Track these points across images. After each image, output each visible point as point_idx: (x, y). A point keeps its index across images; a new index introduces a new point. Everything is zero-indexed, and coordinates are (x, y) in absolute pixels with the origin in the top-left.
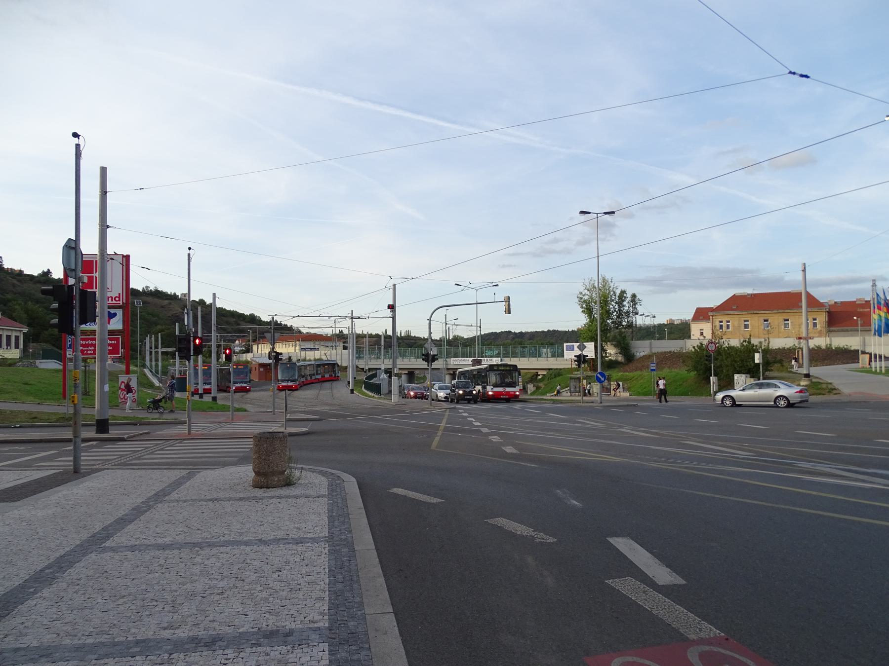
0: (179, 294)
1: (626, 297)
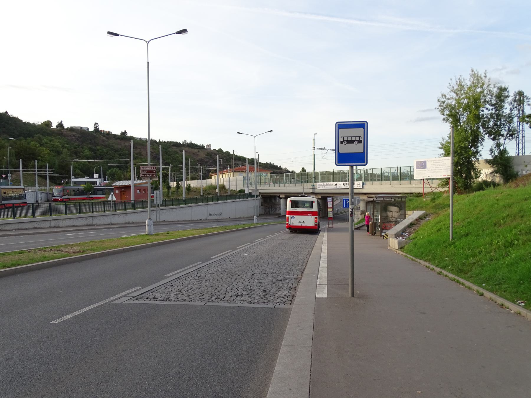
0: (205, 145)
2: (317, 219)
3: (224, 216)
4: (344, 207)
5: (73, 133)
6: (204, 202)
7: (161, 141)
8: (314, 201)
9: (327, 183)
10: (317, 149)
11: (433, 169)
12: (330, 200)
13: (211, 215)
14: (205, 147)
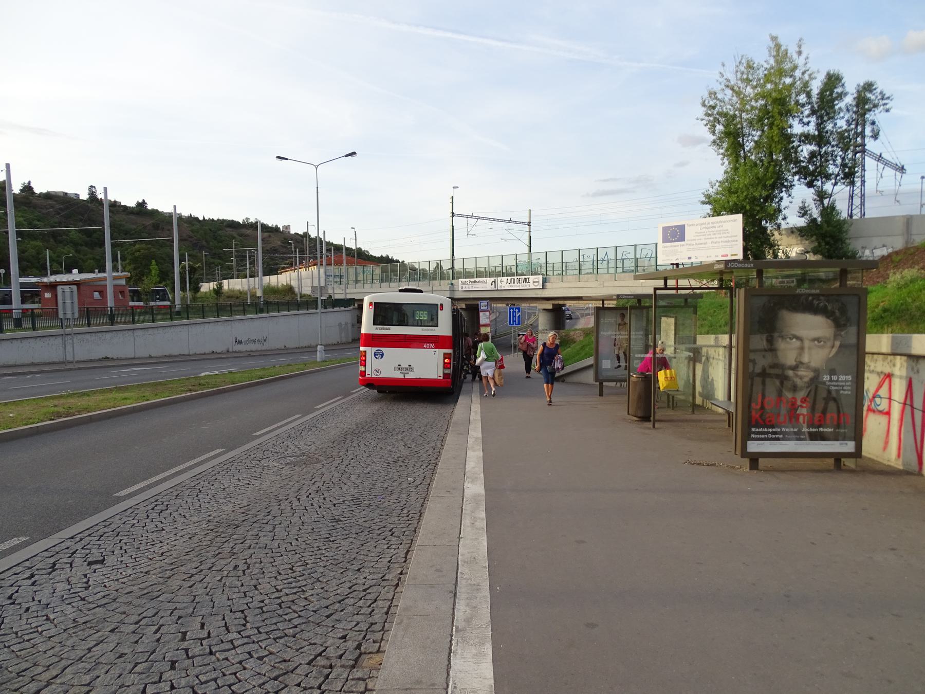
0: (280, 226)
1: (841, 96)
2: (450, 359)
3: (273, 344)
4: (510, 324)
5: (50, 202)
6: (192, 318)
7: (207, 218)
8: (442, 305)
9: (478, 279)
10: (458, 215)
11: (701, 242)
12: (484, 308)
13: (240, 342)
14: (281, 230)
